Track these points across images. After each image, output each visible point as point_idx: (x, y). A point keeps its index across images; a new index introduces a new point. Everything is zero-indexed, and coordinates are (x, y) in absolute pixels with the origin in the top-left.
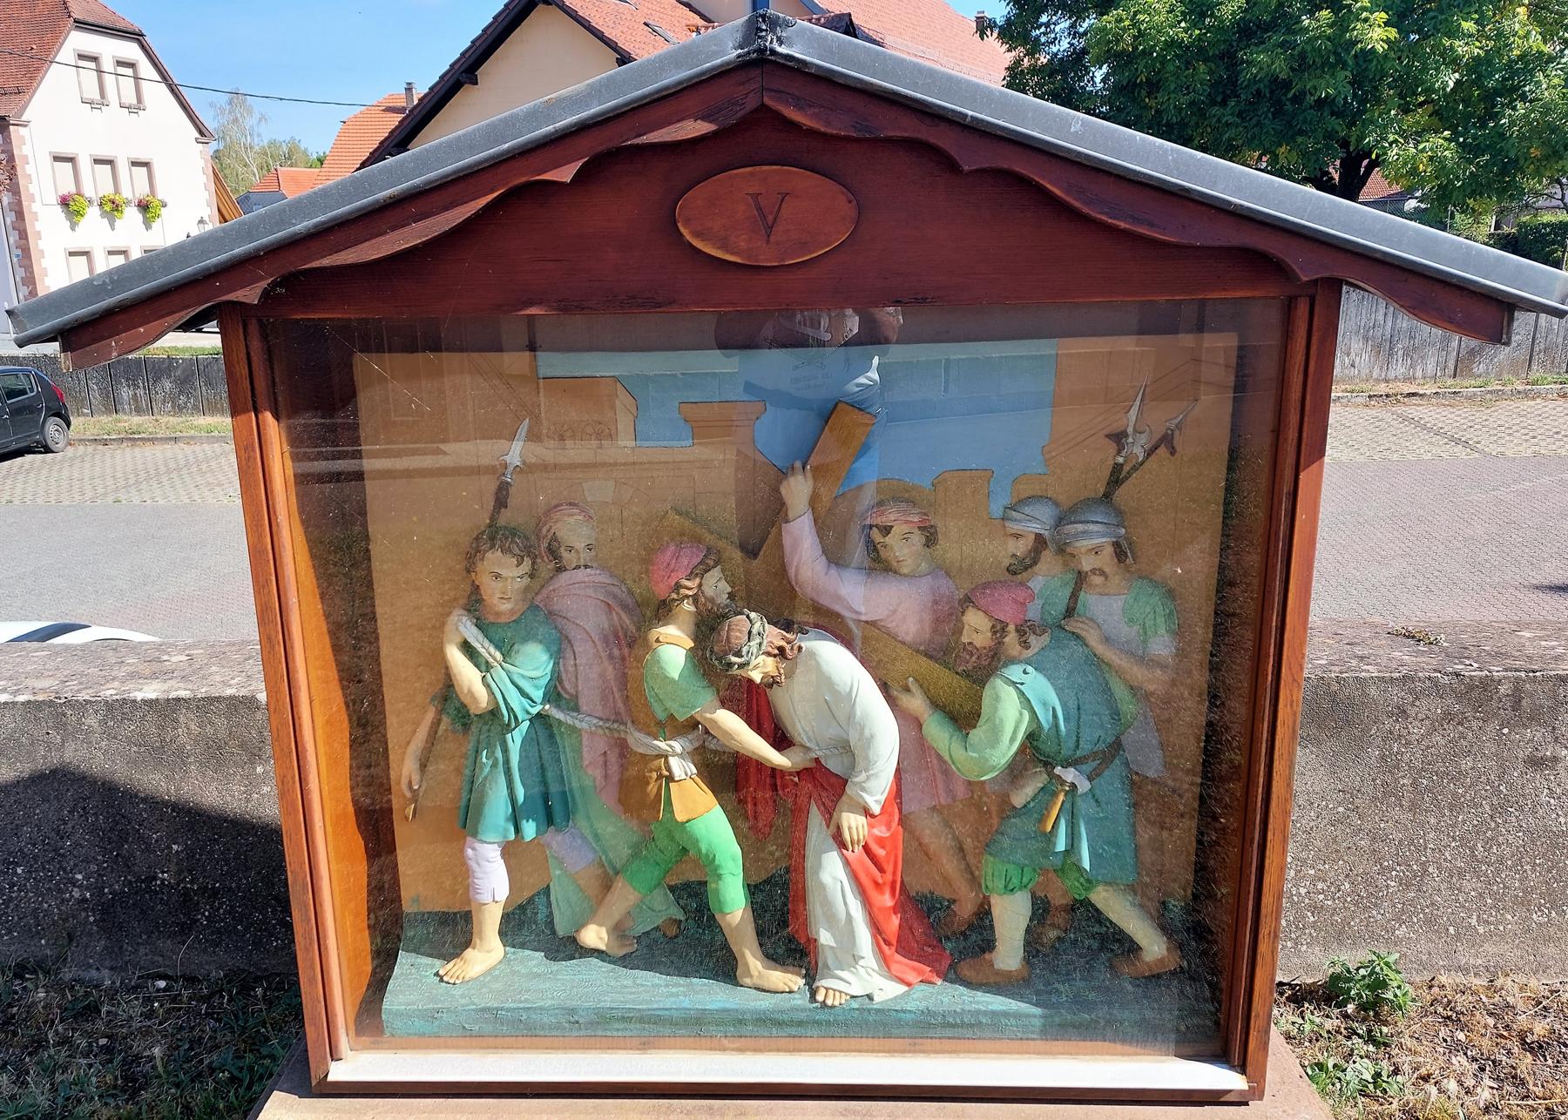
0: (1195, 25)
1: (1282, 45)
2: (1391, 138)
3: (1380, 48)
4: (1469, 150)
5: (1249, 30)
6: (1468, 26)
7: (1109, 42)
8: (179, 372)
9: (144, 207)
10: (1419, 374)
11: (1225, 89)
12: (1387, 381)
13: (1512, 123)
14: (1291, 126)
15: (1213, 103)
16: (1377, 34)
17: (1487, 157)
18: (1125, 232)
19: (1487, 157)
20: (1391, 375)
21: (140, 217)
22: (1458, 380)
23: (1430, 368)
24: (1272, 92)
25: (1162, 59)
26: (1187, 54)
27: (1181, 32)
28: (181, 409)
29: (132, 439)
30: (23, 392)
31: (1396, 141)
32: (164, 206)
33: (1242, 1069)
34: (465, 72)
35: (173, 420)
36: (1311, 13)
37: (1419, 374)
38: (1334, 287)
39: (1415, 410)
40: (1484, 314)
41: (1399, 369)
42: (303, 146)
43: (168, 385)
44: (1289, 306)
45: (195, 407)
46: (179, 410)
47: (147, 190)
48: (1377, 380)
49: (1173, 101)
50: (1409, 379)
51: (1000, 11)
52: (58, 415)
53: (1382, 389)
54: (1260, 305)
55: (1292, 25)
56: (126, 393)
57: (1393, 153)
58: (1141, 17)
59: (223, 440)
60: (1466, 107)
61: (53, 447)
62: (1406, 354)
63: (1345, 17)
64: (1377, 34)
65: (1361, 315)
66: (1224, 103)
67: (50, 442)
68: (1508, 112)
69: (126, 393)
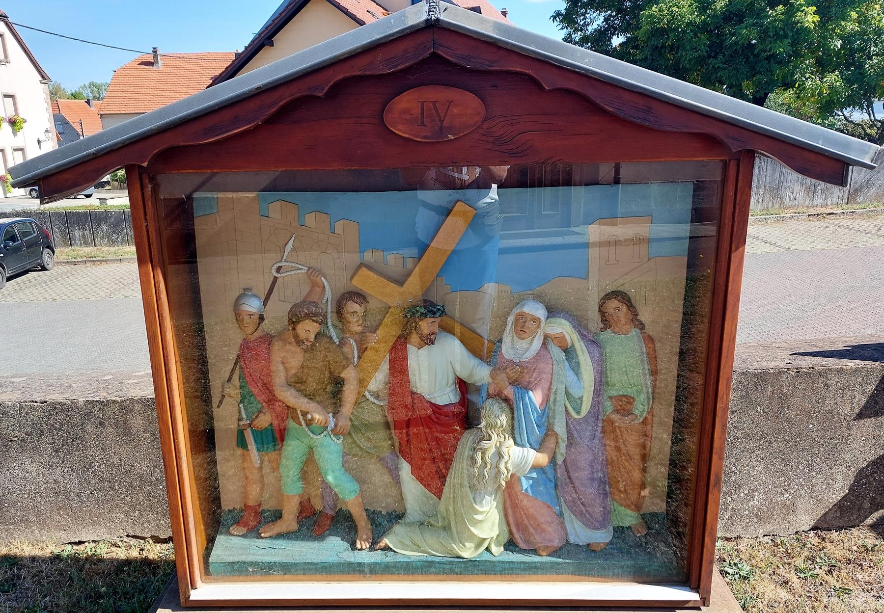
0: (701, 14)
1: (754, 25)
2: (808, 75)
3: (812, 26)
4: (848, 81)
5: (733, 16)
6: (854, 15)
7: (655, 22)
8: (112, 220)
9: (13, 123)
10: (829, 203)
11: (716, 48)
12: (813, 207)
13: (871, 67)
14: (754, 69)
15: (709, 56)
16: (810, 18)
17: (856, 86)
18: (226, 140)
19: (856, 86)
20: (815, 203)
21: (10, 128)
22: (849, 206)
23: (835, 200)
24: (743, 51)
25: (684, 31)
26: (703, 28)
27: (697, 18)
28: (113, 242)
29: (91, 260)
30: (30, 233)
31: (810, 77)
32: (25, 121)
33: (696, 589)
34: (265, 40)
35: (112, 249)
36: (772, 8)
37: (829, 203)
38: (750, 155)
39: (832, 220)
40: (831, 169)
41: (819, 200)
42: (62, 86)
43: (105, 228)
44: (725, 166)
45: (123, 241)
46: (113, 243)
47: (13, 113)
48: (808, 207)
49: (687, 56)
50: (826, 206)
51: (563, 6)
52: (49, 247)
53: (812, 211)
54: (710, 167)
55: (760, 14)
56: (77, 233)
57: (809, 83)
58: (674, 9)
59: (129, 260)
60: (837, 59)
61: (47, 267)
62: (822, 192)
63: (792, 10)
64: (810, 18)
65: (766, 170)
66: (715, 57)
67: (45, 264)
68: (868, 61)
69: (77, 233)
